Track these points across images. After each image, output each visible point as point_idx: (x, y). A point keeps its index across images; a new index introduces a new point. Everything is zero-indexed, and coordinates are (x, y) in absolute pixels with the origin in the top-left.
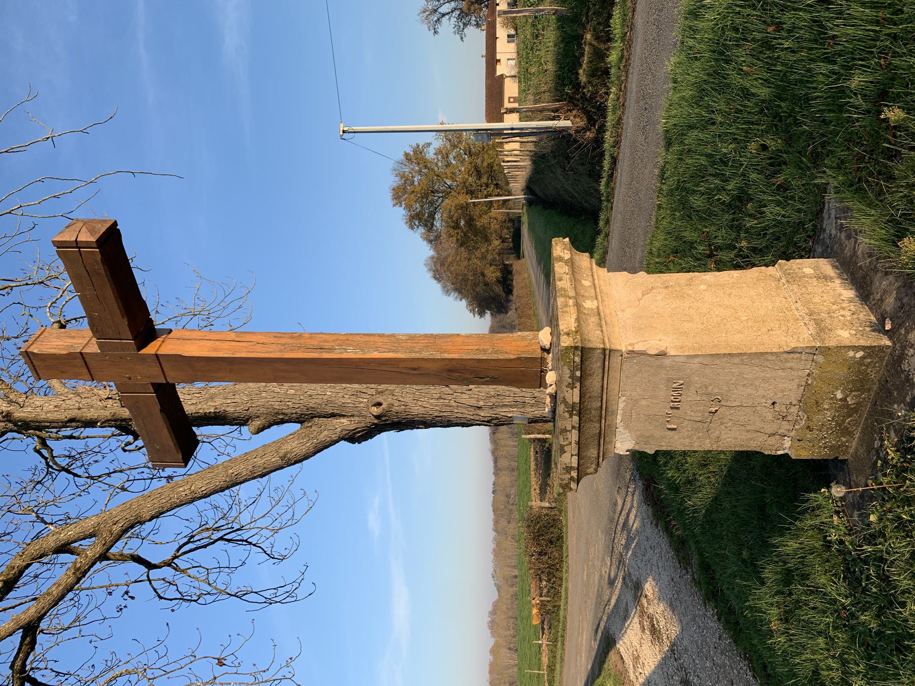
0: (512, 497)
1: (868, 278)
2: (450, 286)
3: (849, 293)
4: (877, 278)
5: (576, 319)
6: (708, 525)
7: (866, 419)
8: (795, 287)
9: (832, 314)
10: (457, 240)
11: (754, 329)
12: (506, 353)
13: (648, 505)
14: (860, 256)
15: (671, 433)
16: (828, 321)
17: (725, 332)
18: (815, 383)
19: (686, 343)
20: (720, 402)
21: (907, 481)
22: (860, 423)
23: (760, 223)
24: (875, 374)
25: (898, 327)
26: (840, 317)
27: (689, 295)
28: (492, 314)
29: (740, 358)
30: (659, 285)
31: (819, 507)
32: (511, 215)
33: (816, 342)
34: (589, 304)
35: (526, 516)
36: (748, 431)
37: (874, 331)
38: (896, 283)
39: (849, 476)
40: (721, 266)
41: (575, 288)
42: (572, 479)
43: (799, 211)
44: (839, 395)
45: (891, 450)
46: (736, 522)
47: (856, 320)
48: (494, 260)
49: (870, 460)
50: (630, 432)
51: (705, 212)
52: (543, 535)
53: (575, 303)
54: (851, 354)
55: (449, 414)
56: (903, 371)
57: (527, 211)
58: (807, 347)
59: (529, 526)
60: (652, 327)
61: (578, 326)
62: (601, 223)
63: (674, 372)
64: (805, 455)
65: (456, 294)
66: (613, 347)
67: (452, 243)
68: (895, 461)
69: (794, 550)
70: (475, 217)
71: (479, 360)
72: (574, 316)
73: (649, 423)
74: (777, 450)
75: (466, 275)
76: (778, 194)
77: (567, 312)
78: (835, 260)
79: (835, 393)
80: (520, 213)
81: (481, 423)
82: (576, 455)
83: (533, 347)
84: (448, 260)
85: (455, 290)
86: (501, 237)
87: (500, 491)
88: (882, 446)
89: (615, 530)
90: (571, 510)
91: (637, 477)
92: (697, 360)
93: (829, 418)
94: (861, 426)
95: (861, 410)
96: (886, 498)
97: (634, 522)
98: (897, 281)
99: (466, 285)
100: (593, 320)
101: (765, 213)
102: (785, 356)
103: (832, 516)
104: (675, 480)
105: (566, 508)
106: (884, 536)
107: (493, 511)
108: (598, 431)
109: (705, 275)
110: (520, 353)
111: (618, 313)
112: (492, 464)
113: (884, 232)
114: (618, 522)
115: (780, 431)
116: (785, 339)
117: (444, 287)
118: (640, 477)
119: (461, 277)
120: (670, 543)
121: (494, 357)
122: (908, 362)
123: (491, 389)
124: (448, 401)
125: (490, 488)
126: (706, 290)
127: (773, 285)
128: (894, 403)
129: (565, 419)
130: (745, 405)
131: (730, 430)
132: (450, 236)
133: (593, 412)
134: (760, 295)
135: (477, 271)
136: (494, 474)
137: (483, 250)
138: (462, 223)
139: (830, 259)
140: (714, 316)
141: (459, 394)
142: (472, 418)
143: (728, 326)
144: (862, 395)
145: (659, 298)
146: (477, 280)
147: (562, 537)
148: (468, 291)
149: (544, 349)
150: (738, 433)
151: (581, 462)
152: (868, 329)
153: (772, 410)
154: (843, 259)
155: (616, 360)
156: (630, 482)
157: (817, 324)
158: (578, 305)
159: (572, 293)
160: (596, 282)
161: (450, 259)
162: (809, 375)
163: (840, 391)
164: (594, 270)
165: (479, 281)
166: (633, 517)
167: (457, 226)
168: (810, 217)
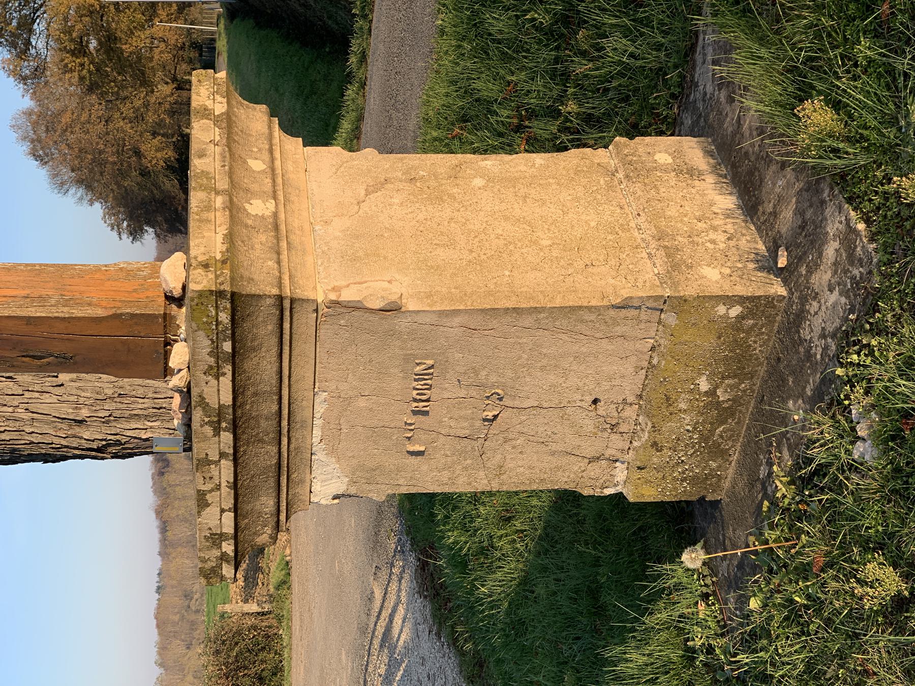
0: (196, 597)
1: (757, 174)
2: (66, 173)
3: (727, 201)
4: (769, 174)
5: (225, 235)
6: (513, 628)
7: (748, 428)
8: (638, 187)
9: (696, 239)
10: (82, 79)
11: (562, 263)
12: (89, 304)
13: (425, 597)
14: (747, 134)
15: (413, 460)
16: (687, 251)
17: (510, 267)
18: (664, 362)
19: (439, 288)
20: (501, 399)
21: (803, 536)
22: (738, 435)
23: (597, 69)
24: (761, 346)
25: (797, 263)
26: (708, 244)
27: (453, 197)
28: (158, 235)
29: (534, 316)
30: (400, 174)
31: (678, 587)
32: (195, 36)
33: (664, 289)
34: (259, 208)
35: (212, 632)
36: (553, 454)
37: (761, 269)
38: (797, 184)
39: (723, 530)
40: (536, 145)
41: (231, 174)
42: (223, 557)
43: (659, 47)
44: (704, 386)
45: (781, 481)
46: (555, 622)
47: (734, 249)
48: (160, 124)
49: (753, 501)
50: (338, 461)
51: (510, 43)
52: (246, 668)
53: (228, 204)
54: (721, 310)
55: (14, 436)
56: (802, 341)
57: (226, 28)
58: (649, 297)
59: (217, 652)
60: (378, 256)
61: (227, 250)
62: (353, 59)
63: (414, 343)
64: (650, 494)
65: (81, 191)
66: (299, 294)
67: (71, 85)
68: (786, 501)
69: (640, 668)
70: (119, 34)
71: (29, 320)
72: (223, 230)
73: (374, 441)
74: (603, 488)
75: (101, 152)
76: (627, 14)
77: (208, 221)
78: (710, 140)
79: (697, 382)
80: (213, 33)
81: (84, 453)
82: (229, 510)
83: (150, 294)
84: (63, 120)
85: (80, 182)
86: (174, 79)
87: (172, 587)
88: (770, 474)
89: (370, 648)
90: (298, 615)
91: (408, 547)
92: (457, 320)
93: (689, 428)
94: (741, 440)
95: (740, 412)
96: (775, 568)
97: (401, 631)
98: (798, 181)
99: (101, 174)
100: (264, 239)
101: (603, 48)
102: (612, 313)
103: (697, 603)
104: (461, 549)
105: (290, 612)
106: (769, 635)
107: (158, 626)
108: (274, 461)
109: (485, 159)
110: (120, 304)
111: (317, 228)
112: (156, 535)
113: (779, 89)
114: (374, 632)
115: (608, 453)
116: (613, 281)
117: (55, 176)
118: (412, 545)
119: (90, 157)
120: (461, 666)
121: (64, 312)
122: (810, 325)
123: (105, 382)
124: (10, 409)
125: (153, 582)
126: (484, 188)
127: (602, 182)
128: (788, 398)
129: (205, 438)
130: (545, 405)
132: (66, 70)
133: (263, 424)
134: (577, 199)
135: (124, 145)
136: (160, 554)
137: (138, 103)
138: (93, 44)
139: (702, 139)
140: (493, 236)
141: (37, 395)
142: (64, 442)
143: (517, 256)
144: (740, 384)
145: (396, 201)
146: (125, 165)
147: (282, 670)
148: (106, 185)
149: (169, 298)
150: (535, 458)
151: (243, 523)
152: (751, 266)
153: (593, 414)
154: (722, 139)
155: (305, 321)
156: (394, 556)
157: (668, 256)
158: (234, 210)
159: (223, 184)
160: (278, 163)
161: (66, 119)
162: (653, 349)
163: (704, 378)
164: (276, 141)
165: (130, 166)
166: (400, 621)
167: (80, 50)
168: (674, 60)
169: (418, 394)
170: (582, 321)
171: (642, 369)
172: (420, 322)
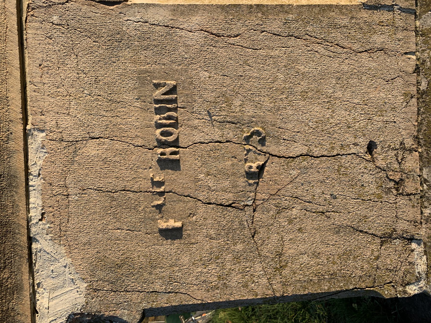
63: (149, 53)
115: (402, 226)
130: (316, 152)
131: (300, 230)
150: (318, 238)
153: (370, 165)
169: (162, 134)
170: (336, 26)
171: (412, 97)
172: (151, 21)
